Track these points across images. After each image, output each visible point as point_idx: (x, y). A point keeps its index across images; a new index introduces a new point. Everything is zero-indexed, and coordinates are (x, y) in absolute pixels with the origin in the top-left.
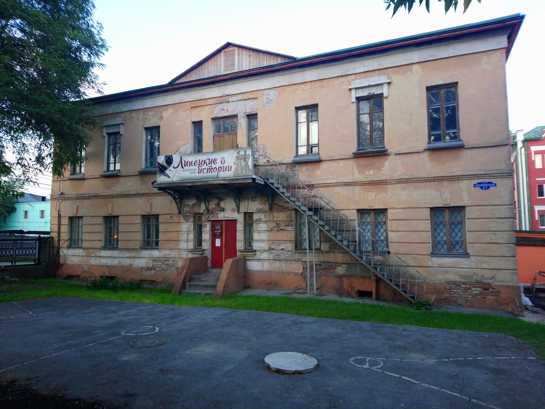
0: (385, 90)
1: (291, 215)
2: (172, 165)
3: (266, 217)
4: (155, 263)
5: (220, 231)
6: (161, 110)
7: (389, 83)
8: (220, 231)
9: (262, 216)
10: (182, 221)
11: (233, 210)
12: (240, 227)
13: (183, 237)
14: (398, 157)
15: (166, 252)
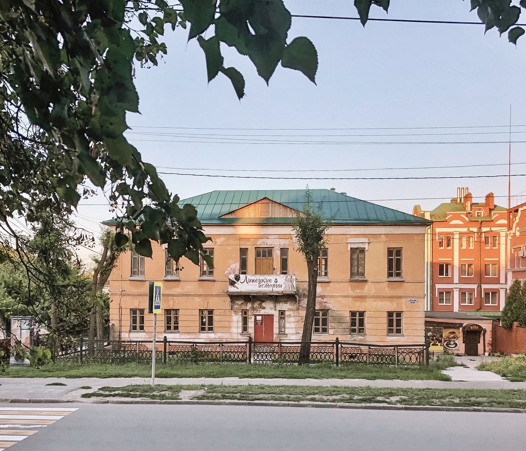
0: (366, 246)
2: (240, 281)
5: (260, 322)
6: (215, 237)
8: (260, 322)
10: (233, 314)
11: (271, 308)
12: (276, 319)
13: (234, 324)
14: (372, 284)
15: (221, 335)
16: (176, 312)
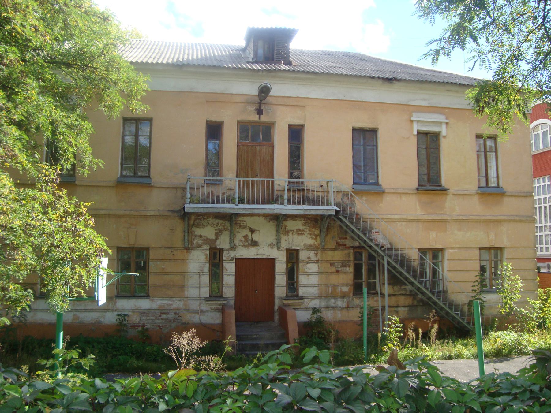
0: (444, 130)
1: (349, 253)
3: (316, 256)
4: (144, 318)
7: (447, 123)
9: (312, 254)
11: (271, 245)
12: (281, 268)
13: (192, 281)
15: (164, 302)
16: (496, 256)
